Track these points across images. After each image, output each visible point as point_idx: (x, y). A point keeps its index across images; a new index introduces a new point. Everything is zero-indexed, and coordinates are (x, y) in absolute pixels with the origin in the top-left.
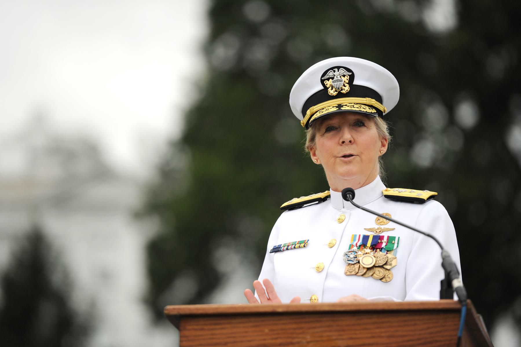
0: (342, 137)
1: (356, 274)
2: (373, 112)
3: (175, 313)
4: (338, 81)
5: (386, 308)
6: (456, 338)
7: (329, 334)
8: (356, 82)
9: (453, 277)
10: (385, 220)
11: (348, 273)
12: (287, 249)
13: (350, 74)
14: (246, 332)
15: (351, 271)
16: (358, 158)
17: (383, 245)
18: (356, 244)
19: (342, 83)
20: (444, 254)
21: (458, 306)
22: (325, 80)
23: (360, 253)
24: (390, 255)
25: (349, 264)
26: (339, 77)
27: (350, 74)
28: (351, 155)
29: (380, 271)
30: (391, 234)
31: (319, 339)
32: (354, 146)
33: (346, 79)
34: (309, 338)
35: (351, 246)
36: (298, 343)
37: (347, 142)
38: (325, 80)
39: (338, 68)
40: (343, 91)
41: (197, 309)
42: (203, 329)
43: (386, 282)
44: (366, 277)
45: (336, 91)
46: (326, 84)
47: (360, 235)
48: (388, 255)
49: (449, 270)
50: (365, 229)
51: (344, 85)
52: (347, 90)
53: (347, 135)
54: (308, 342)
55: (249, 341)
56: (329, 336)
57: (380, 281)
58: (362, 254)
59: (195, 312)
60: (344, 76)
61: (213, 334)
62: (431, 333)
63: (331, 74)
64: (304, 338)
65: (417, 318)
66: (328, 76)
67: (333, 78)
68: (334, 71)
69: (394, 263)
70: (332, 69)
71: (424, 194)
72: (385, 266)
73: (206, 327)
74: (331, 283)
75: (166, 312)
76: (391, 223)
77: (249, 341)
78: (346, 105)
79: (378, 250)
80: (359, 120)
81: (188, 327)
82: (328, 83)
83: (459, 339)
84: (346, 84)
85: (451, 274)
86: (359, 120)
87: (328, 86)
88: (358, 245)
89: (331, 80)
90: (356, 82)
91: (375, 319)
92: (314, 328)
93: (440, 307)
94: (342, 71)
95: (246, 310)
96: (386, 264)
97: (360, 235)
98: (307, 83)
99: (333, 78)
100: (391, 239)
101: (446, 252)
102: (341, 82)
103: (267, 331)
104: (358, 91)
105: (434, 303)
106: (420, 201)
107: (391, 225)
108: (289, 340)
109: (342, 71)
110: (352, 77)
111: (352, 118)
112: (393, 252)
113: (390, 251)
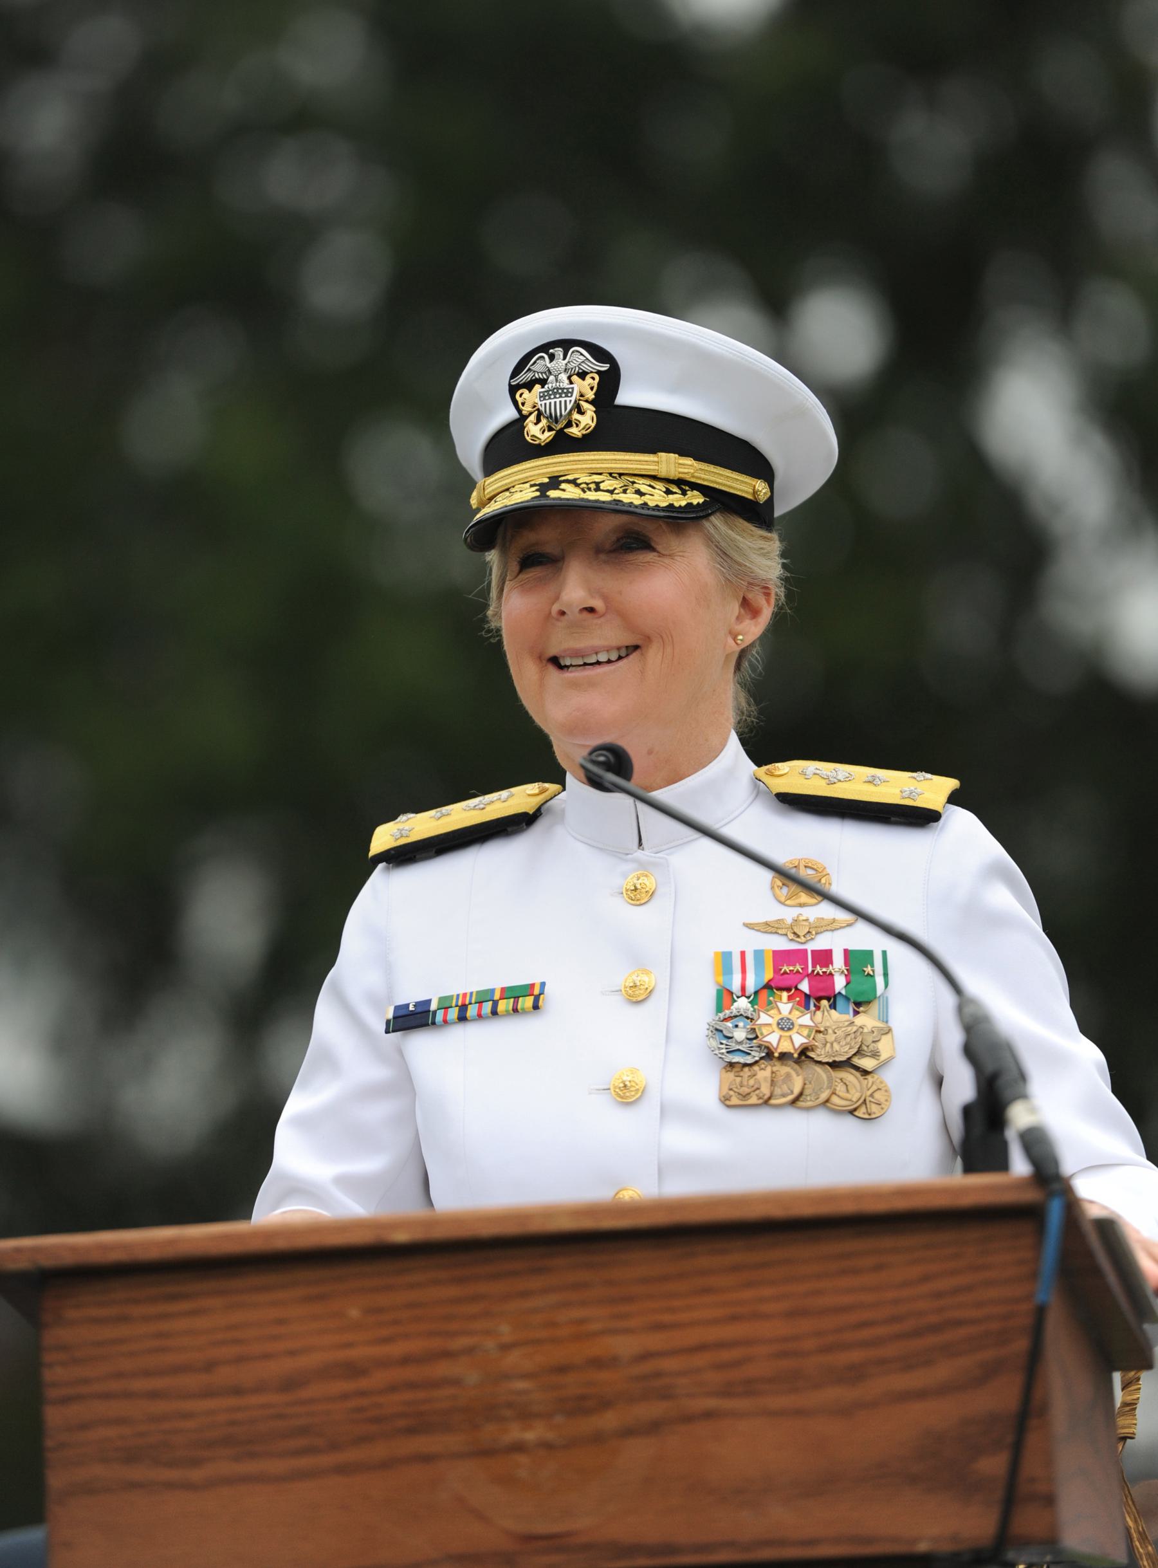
0: (557, 598)
1: (766, 1102)
2: (695, 502)
3: (22, 1264)
5: (777, 1212)
7: (577, 1313)
8: (627, 396)
11: (735, 1100)
12: (462, 1018)
13: (605, 367)
14: (281, 1322)
15: (745, 1090)
17: (840, 983)
18: (743, 988)
19: (570, 402)
20: (968, 1010)
21: (1031, 1196)
22: (519, 387)
23: (764, 1019)
25: (731, 1065)
26: (564, 377)
27: (605, 367)
29: (840, 1076)
33: (587, 387)
34: (505, 1331)
35: (725, 997)
36: (470, 1351)
37: (573, 614)
38: (519, 387)
39: (566, 344)
40: (575, 431)
41: (104, 1247)
42: (124, 1319)
43: (870, 1119)
44: (808, 1109)
45: (550, 429)
46: (520, 400)
47: (743, 954)
48: (860, 1020)
49: (990, 1068)
50: (746, 925)
52: (586, 428)
54: (505, 1348)
55: (292, 1353)
56: (581, 1322)
57: (850, 1121)
58: (773, 1022)
59: (96, 1258)
60: (582, 375)
61: (160, 1335)
62: (939, 1295)
63: (540, 365)
65: (887, 1242)
66: (530, 375)
67: (543, 382)
68: (552, 357)
70: (545, 348)
71: (931, 789)
72: (856, 1061)
74: (682, 1140)
77: (292, 1353)
78: (574, 482)
79: (824, 1003)
80: (633, 537)
81: (71, 1314)
83: (1040, 1313)
84: (585, 405)
85: (1001, 1082)
86: (633, 537)
87: (526, 410)
88: (751, 987)
89: (537, 388)
90: (627, 396)
91: (738, 1254)
92: (525, 1294)
93: (966, 1201)
94: (580, 358)
96: (859, 1053)
97: (743, 954)
98: (481, 395)
99: (543, 382)
100: (857, 961)
101: (972, 1001)
102: (571, 391)
103: (354, 1313)
106: (920, 818)
109: (580, 358)
110: (610, 381)
111: (606, 526)
112: (875, 1008)
113: (869, 1002)
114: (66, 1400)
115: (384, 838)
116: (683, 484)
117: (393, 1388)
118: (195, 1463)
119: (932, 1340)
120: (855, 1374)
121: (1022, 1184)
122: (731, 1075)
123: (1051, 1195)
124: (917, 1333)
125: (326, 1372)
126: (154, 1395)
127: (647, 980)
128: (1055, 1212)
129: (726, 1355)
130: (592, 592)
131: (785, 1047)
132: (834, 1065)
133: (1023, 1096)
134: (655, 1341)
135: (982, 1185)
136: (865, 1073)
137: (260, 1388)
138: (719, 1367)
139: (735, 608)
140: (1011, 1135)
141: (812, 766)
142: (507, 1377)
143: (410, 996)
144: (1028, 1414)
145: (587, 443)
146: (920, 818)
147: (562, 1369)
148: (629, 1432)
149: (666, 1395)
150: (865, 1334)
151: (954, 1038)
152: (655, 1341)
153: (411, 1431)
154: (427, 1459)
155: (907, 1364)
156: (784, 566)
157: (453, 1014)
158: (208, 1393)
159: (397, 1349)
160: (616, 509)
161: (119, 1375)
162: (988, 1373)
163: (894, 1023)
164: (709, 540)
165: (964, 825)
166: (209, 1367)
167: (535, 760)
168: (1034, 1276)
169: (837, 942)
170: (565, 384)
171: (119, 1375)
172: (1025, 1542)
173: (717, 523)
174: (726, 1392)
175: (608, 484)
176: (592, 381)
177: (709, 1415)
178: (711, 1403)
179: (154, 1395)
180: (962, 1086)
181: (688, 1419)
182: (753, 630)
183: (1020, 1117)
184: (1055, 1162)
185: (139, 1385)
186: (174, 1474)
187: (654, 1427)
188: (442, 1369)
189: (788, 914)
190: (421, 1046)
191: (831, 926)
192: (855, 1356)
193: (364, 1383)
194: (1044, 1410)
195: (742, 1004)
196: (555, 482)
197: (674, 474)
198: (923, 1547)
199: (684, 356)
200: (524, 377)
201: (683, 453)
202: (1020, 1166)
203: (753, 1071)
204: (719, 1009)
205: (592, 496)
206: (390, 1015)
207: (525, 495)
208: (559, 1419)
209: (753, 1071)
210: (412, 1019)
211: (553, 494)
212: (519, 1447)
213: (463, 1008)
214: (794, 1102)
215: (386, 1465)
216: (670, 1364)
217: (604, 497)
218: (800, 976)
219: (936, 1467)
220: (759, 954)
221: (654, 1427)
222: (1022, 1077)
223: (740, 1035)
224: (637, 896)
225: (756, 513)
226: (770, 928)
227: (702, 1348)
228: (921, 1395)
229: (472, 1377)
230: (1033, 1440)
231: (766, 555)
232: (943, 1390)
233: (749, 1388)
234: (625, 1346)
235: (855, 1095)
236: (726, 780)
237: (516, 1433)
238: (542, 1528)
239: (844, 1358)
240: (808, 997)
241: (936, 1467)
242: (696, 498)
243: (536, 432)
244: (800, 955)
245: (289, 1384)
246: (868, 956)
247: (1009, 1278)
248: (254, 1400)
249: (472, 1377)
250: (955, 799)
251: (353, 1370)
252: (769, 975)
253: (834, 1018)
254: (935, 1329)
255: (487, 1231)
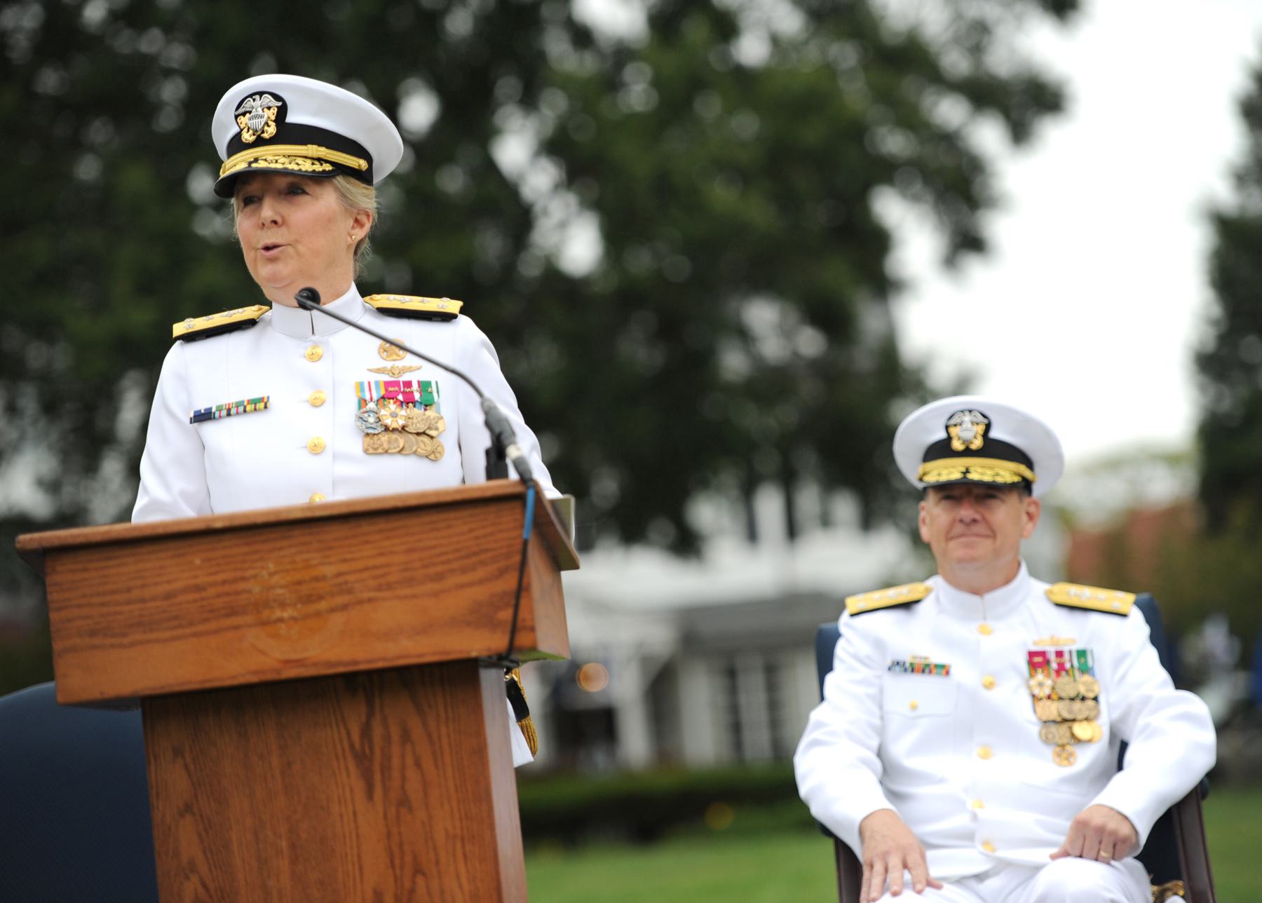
3: (35, 545)
4: (257, 117)
6: (519, 541)
7: (305, 556)
8: (291, 118)
9: (506, 442)
10: (397, 350)
12: (229, 414)
13: (280, 104)
16: (290, 249)
17: (417, 396)
20: (486, 404)
21: (520, 489)
23: (383, 412)
24: (431, 413)
25: (368, 434)
27: (280, 104)
28: (275, 247)
29: (420, 440)
30: (424, 378)
31: (289, 567)
32: (283, 230)
33: (272, 114)
35: (362, 402)
36: (255, 577)
37: (268, 223)
39: (261, 94)
40: (266, 136)
41: (72, 536)
42: (85, 570)
43: (435, 460)
49: (497, 430)
51: (267, 124)
53: (268, 210)
54: (271, 574)
59: (70, 541)
60: (269, 108)
62: (477, 538)
64: (263, 568)
65: (452, 515)
69: (440, 425)
70: (251, 96)
71: (453, 306)
73: (110, 563)
74: (343, 469)
75: (18, 546)
76: (409, 356)
77: (169, 582)
80: (295, 186)
82: (953, 431)
85: (503, 437)
86: (295, 186)
88: (375, 398)
90: (291, 118)
91: (382, 524)
92: (280, 549)
93: (489, 493)
94: (267, 99)
95: (160, 531)
100: (424, 386)
101: (488, 400)
102: (263, 118)
103: (198, 562)
104: (288, 133)
105: (480, 489)
106: (447, 317)
107: (410, 360)
108: (238, 574)
109: (267, 99)
110: (283, 111)
111: (282, 182)
114: (59, 609)
115: (179, 329)
116: (320, 160)
117: (218, 596)
118: (124, 635)
119: (475, 559)
120: (440, 577)
121: (515, 484)
122: (368, 439)
123: (528, 488)
124: (468, 556)
125: (186, 590)
126: (103, 604)
127: (323, 396)
128: (530, 496)
129: (378, 572)
130: (276, 213)
131: (395, 425)
132: (418, 434)
133: (514, 443)
134: (343, 567)
135: (497, 486)
136: (432, 437)
137: (154, 599)
138: (375, 577)
139: (351, 222)
140: (509, 462)
141: (392, 296)
142: (273, 587)
143: (202, 407)
144: (521, 590)
145: (273, 141)
146: (447, 317)
147: (299, 583)
148: (333, 610)
149: (350, 592)
150: (443, 558)
151: (480, 418)
152: (343, 567)
153: (228, 615)
154: (236, 628)
155: (464, 571)
156: (378, 203)
157: (224, 413)
158: (129, 602)
159: (220, 577)
160: (285, 173)
161: (84, 596)
162: (501, 573)
163: (443, 414)
164: (337, 189)
165: (465, 322)
166: (129, 590)
167: (255, 295)
168: (522, 526)
169: (414, 378)
170: (260, 112)
171: (84, 596)
172: (521, 650)
173: (340, 181)
174: (379, 588)
175: (282, 160)
176: (274, 111)
177: (370, 600)
178: (372, 594)
179: (103, 604)
180: (485, 441)
181: (360, 602)
182: (360, 233)
183: (512, 452)
184: (530, 472)
185: (94, 600)
186: (114, 641)
187: (345, 607)
188: (242, 586)
189: (389, 364)
190: (208, 428)
191: (410, 369)
192: (439, 569)
193: (204, 594)
194: (528, 589)
195: (371, 406)
196: (256, 160)
197: (315, 155)
198: (474, 654)
199: (317, 100)
200: (241, 110)
201: (320, 145)
202: (513, 475)
203: (378, 437)
204: (360, 408)
205: (273, 166)
206: (192, 415)
207: (242, 166)
208: (299, 606)
209: (378, 437)
210: (203, 417)
211: (254, 165)
212: (281, 620)
213: (229, 410)
214: (400, 452)
215: (216, 632)
216: (351, 578)
217: (279, 166)
218: (398, 393)
219: (480, 617)
220: (377, 383)
221: (345, 607)
222: (513, 434)
223: (372, 420)
224: (314, 358)
225: (365, 177)
226: (379, 371)
227: (366, 569)
228: (471, 584)
229: (256, 589)
230: (523, 602)
231: (366, 196)
232: (481, 582)
233: (389, 586)
234: (329, 570)
235: (429, 448)
236: (350, 302)
237: (278, 613)
238: (293, 656)
239: (433, 570)
240: (402, 403)
241: (480, 617)
242: (328, 167)
243: (247, 137)
244: (397, 383)
245: (168, 596)
246: (428, 384)
247: (512, 528)
248: (150, 605)
249: (256, 589)
250: (463, 311)
251: (198, 588)
252: (383, 392)
253: (417, 412)
254: (475, 554)
255: (260, 520)
